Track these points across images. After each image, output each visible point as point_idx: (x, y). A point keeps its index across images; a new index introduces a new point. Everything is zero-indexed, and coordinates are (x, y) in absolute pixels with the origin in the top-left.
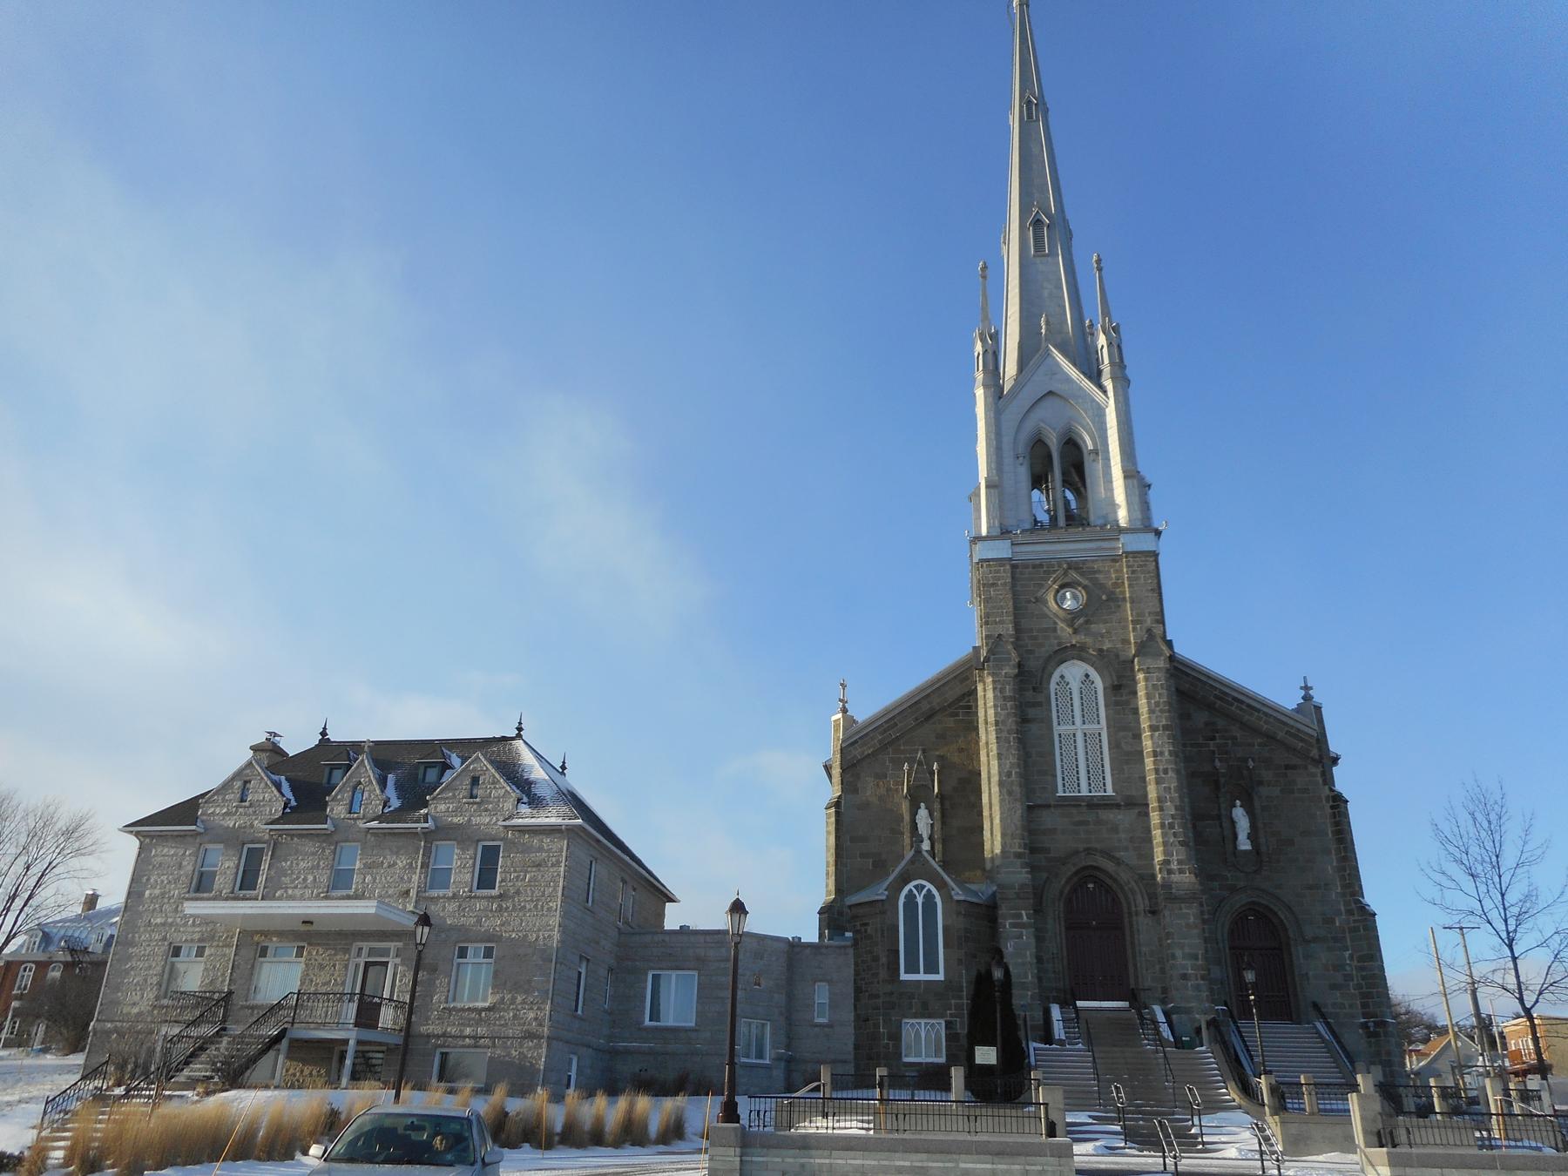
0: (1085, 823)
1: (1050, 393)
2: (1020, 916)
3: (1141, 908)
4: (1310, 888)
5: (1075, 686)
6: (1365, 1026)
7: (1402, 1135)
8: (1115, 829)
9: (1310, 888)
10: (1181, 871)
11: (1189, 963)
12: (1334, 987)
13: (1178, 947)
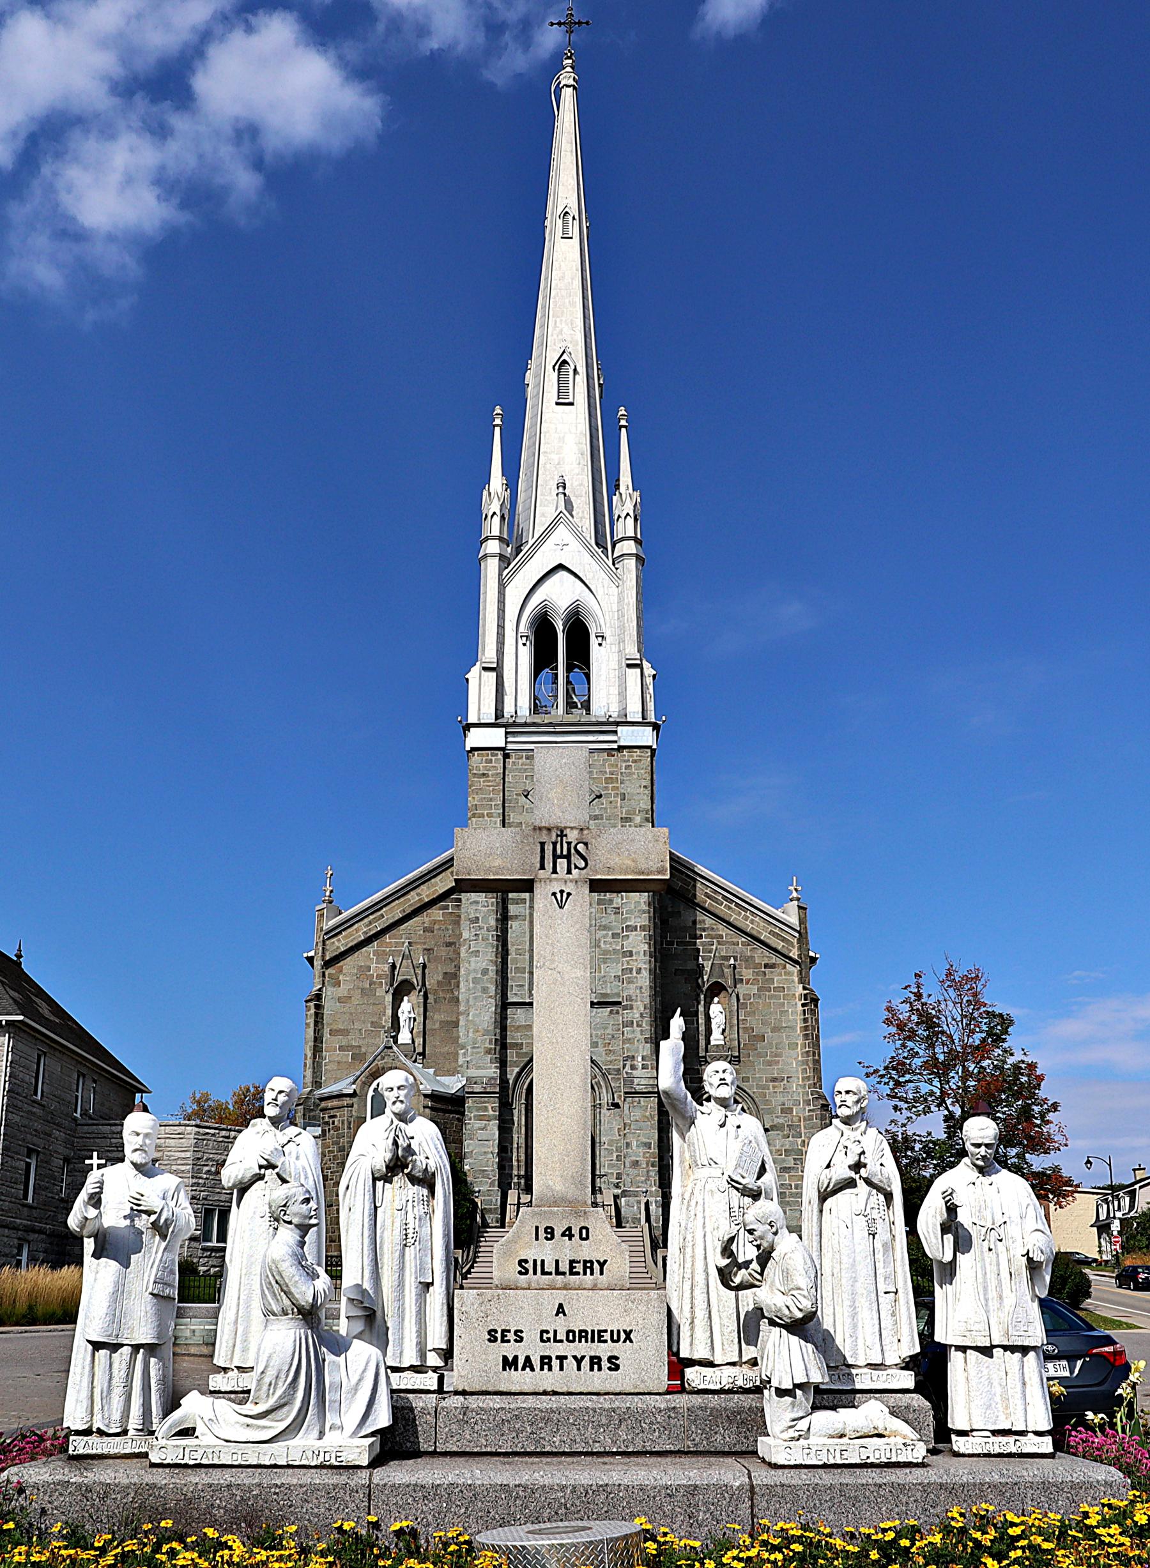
1: (561, 567)
4: (774, 1080)
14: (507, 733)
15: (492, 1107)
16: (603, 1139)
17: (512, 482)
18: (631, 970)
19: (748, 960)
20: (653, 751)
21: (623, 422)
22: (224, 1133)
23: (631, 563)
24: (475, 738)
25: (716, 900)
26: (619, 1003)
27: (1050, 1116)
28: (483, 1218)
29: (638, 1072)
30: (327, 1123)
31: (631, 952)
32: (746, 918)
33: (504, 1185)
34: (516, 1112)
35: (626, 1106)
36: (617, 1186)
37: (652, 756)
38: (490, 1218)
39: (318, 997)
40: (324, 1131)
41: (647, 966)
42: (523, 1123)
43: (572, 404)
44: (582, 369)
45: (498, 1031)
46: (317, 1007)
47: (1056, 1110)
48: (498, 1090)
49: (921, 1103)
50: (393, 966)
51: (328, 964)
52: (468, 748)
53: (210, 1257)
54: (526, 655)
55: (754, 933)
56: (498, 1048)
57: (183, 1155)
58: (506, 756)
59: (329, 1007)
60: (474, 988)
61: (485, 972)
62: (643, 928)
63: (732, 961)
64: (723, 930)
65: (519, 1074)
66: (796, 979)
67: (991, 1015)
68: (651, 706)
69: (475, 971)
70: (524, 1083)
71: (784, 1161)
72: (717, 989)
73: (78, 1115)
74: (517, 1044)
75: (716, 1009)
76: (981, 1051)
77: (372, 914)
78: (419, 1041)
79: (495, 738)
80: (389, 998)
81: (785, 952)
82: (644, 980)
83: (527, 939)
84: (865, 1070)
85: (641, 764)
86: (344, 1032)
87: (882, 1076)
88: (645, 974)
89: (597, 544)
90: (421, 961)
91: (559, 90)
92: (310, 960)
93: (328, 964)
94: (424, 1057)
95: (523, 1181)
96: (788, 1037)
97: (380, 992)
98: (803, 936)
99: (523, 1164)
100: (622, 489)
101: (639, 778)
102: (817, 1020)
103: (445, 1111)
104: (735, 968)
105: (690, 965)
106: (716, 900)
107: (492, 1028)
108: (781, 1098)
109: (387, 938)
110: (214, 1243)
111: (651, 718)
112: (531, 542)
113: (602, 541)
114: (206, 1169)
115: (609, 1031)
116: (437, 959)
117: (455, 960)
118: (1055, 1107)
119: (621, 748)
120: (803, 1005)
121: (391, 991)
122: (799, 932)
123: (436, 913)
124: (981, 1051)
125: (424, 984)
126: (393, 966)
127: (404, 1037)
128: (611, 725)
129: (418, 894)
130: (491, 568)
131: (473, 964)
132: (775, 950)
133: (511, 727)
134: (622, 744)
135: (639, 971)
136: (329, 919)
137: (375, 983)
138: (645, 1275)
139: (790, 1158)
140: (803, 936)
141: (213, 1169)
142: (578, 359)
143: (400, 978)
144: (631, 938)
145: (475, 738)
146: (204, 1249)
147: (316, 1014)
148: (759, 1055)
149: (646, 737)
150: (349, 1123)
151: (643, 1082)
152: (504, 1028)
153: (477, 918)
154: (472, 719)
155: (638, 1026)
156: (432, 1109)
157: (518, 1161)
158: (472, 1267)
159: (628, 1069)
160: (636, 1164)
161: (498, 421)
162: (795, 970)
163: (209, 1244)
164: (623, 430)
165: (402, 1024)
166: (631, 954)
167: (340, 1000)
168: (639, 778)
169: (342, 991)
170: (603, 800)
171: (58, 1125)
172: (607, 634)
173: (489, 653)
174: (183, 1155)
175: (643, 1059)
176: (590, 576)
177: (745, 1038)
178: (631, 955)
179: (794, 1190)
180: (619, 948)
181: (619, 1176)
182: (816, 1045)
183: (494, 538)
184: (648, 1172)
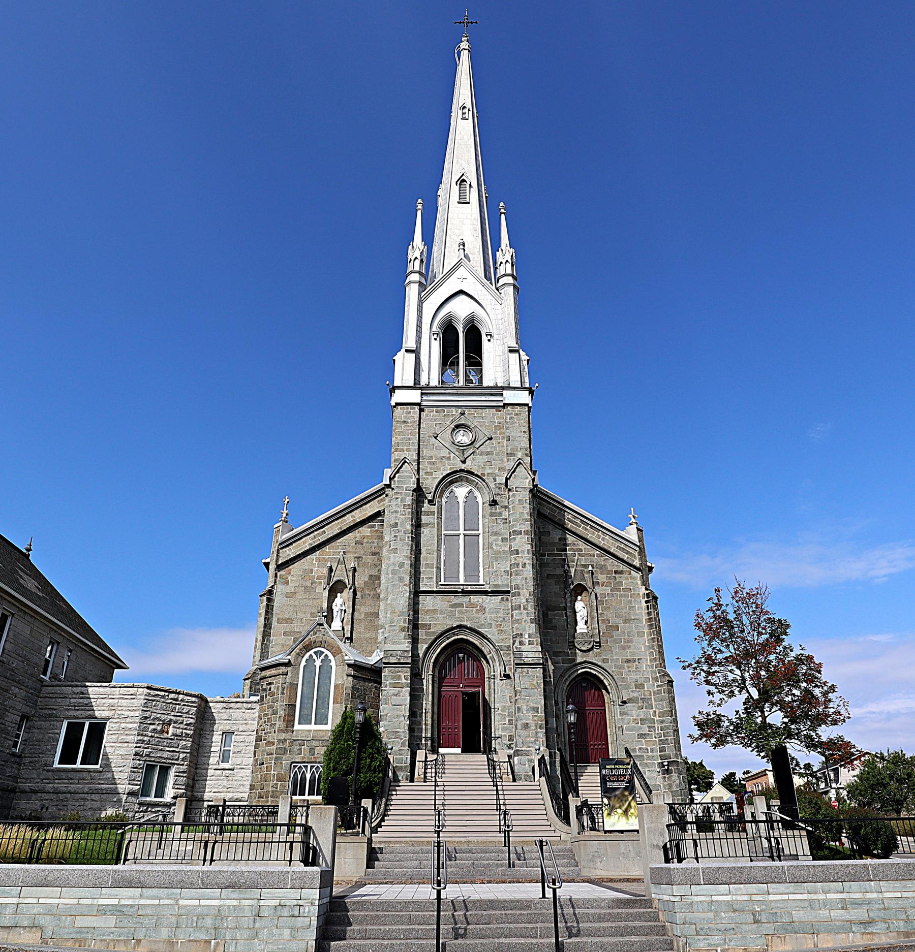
0: (461, 605)
1: (461, 292)
2: (399, 677)
3: (497, 673)
4: (628, 661)
5: (461, 500)
6: (661, 765)
7: (688, 849)
8: (482, 610)
9: (628, 661)
10: (530, 643)
11: (531, 714)
12: (641, 736)
13: (517, 704)
14: (422, 394)
15: (404, 675)
16: (497, 706)
17: (428, 239)
18: (518, 565)
19: (602, 567)
20: (530, 408)
21: (502, 211)
22: (172, 696)
23: (511, 289)
24: (399, 396)
25: (576, 524)
26: (508, 592)
27: (831, 696)
28: (394, 773)
29: (525, 648)
30: (265, 690)
31: (517, 551)
32: (599, 537)
33: (414, 746)
34: (424, 681)
35: (517, 676)
36: (510, 747)
37: (529, 411)
38: (401, 775)
39: (270, 592)
40: (262, 697)
41: (530, 562)
42: (430, 691)
43: (468, 203)
44: (475, 184)
45: (411, 613)
46: (269, 600)
47: (834, 691)
48: (410, 661)
49: (727, 688)
50: (331, 570)
51: (280, 567)
52: (393, 404)
53: (146, 811)
54: (436, 346)
55: (606, 547)
56: (411, 627)
57: (132, 714)
58: (421, 410)
59: (279, 600)
60: (393, 578)
61: (401, 565)
62: (526, 532)
63: (590, 568)
64: (581, 545)
65: (428, 649)
66: (639, 583)
67: (771, 621)
68: (527, 379)
69: (394, 564)
70: (431, 657)
71: (641, 728)
72: (581, 589)
73: (47, 678)
74: (426, 625)
75: (579, 605)
76: (766, 648)
77: (316, 530)
78: (348, 628)
79: (414, 396)
80: (326, 594)
81: (630, 562)
82: (529, 572)
83: (435, 542)
84: (682, 664)
85: (521, 417)
86: (289, 621)
87: (695, 668)
88: (529, 568)
89: (486, 276)
90: (352, 565)
91: (459, 53)
92: (267, 565)
93: (280, 567)
94: (351, 641)
95: (429, 743)
96: (637, 627)
97: (319, 589)
98: (642, 551)
99: (429, 727)
100: (503, 246)
101: (520, 426)
102: (658, 614)
103: (364, 680)
104: (592, 573)
105: (559, 571)
106: (576, 524)
107: (406, 610)
108: (634, 676)
109: (327, 549)
110: (152, 799)
111: (527, 385)
112: (441, 276)
113: (489, 274)
114: (152, 727)
115: (501, 615)
116: (364, 564)
117: (378, 565)
118: (833, 689)
119: (506, 405)
120: (646, 602)
121: (328, 588)
122: (639, 547)
123: (365, 530)
124: (766, 648)
125: (354, 583)
126: (331, 570)
127: (336, 624)
128: (498, 390)
129: (352, 517)
130: (413, 291)
131: (392, 560)
132: (622, 560)
133: (426, 390)
134: (507, 401)
135: (524, 565)
136: (283, 534)
137: (315, 583)
138: (548, 828)
139: (645, 726)
140: (642, 551)
141: (159, 728)
142: (472, 177)
143: (335, 579)
144: (517, 540)
145: (399, 396)
146: (141, 804)
147: (267, 606)
148: (615, 641)
149: (524, 397)
150: (283, 689)
151: (530, 655)
152: (416, 612)
153: (397, 524)
154: (397, 383)
155: (524, 609)
156: (354, 677)
157: (426, 724)
158: (383, 820)
159: (517, 644)
160: (526, 726)
161: (420, 207)
162: (638, 575)
163: (148, 799)
164: (503, 215)
165: (335, 614)
166: (517, 552)
167: (287, 595)
168: (520, 426)
169: (290, 588)
170: (493, 441)
171: (18, 682)
172: (494, 334)
173: (409, 341)
174: (132, 714)
175: (529, 637)
176: (482, 297)
177: (603, 627)
178: (518, 553)
179: (650, 754)
180: (507, 549)
181: (511, 738)
182: (659, 633)
183: (415, 272)
184: (537, 733)
